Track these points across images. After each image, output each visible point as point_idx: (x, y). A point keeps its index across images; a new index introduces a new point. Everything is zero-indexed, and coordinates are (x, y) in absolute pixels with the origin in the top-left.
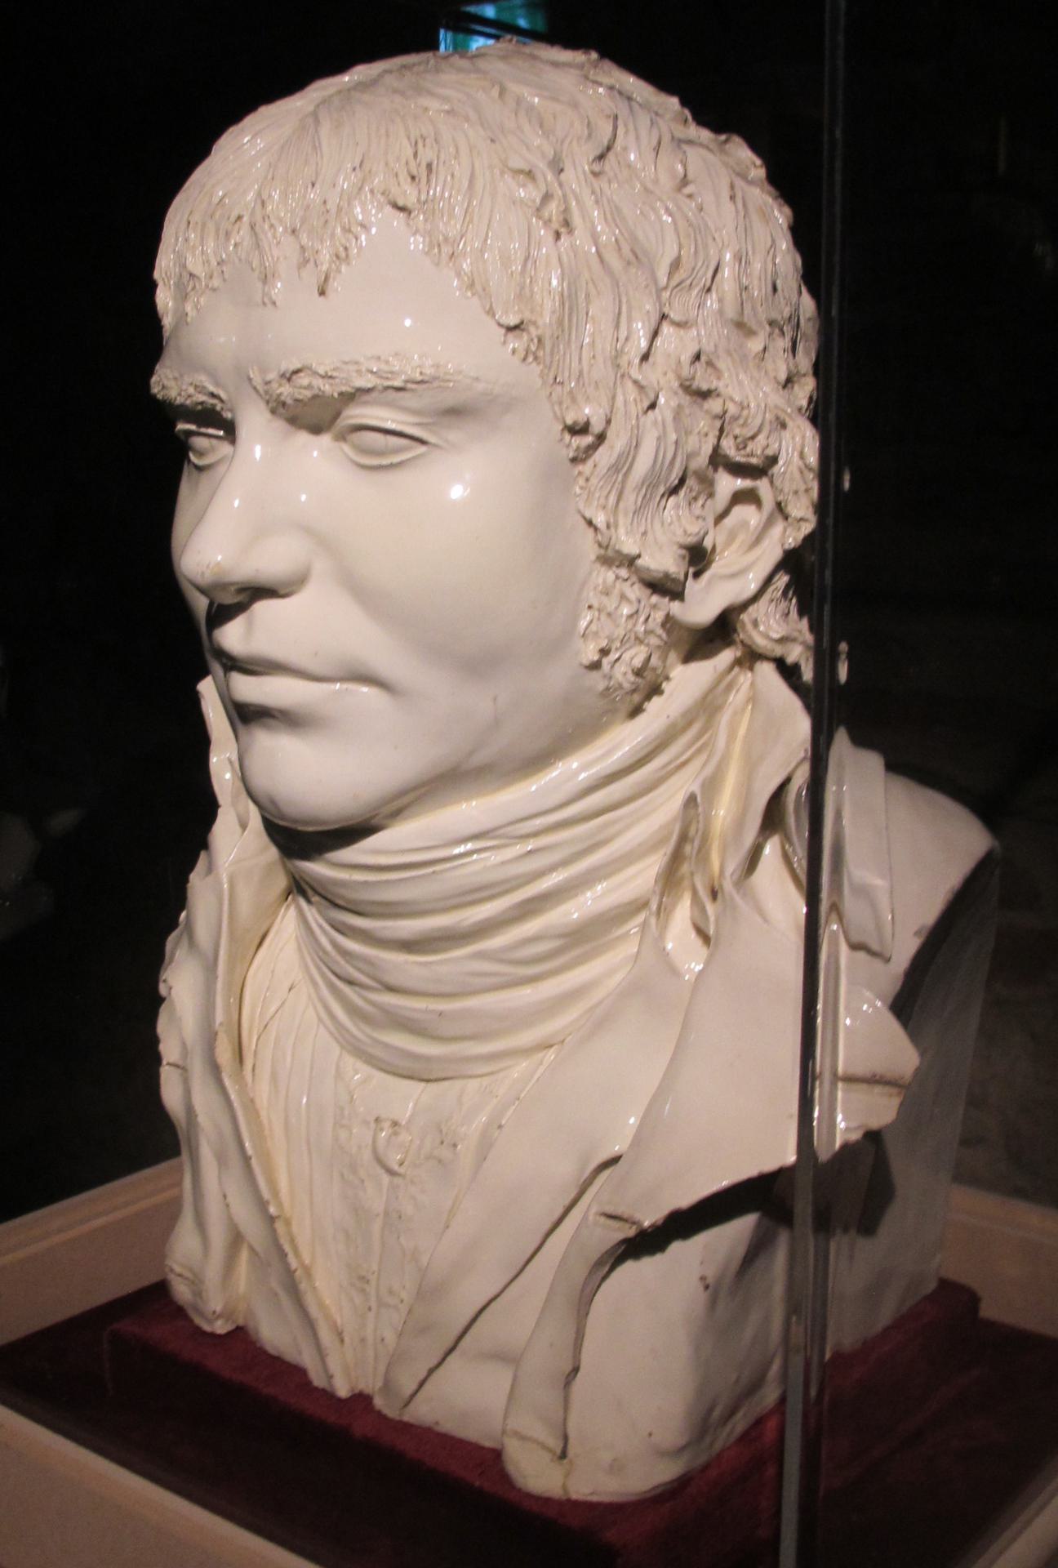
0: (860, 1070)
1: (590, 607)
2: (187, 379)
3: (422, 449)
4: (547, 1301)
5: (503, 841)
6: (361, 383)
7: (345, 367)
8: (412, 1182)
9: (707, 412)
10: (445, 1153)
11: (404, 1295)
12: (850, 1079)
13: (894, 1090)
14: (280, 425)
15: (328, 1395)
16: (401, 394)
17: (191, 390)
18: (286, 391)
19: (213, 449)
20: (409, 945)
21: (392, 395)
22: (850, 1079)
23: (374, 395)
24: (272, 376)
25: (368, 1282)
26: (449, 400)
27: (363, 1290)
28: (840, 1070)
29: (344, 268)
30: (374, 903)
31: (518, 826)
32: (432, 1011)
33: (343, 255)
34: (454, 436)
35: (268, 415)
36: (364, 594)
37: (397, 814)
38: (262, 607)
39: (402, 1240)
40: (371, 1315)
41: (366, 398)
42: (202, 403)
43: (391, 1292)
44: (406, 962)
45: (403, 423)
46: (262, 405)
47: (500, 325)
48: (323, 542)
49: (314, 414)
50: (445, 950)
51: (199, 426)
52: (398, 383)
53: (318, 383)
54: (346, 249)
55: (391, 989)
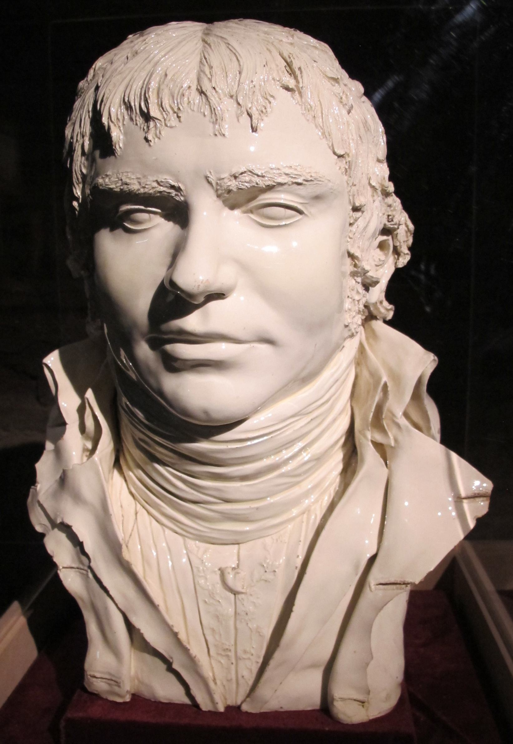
0: (470, 494)
1: (348, 297)
2: (151, 178)
3: (300, 217)
4: (371, 627)
5: (302, 417)
6: (280, 180)
7: (271, 171)
8: (251, 595)
9: (386, 203)
10: (269, 576)
11: (253, 651)
12: (467, 498)
13: (485, 499)
14: (219, 203)
15: (214, 714)
16: (299, 187)
17: (155, 184)
18: (233, 184)
19: (150, 220)
20: (244, 478)
21: (295, 186)
22: (467, 498)
23: (285, 187)
24: (226, 175)
25: (230, 650)
26: (318, 191)
27: (228, 656)
28: (463, 494)
29: (265, 118)
30: (239, 458)
31: (307, 408)
32: (253, 508)
33: (264, 111)
34: (313, 210)
35: (215, 198)
36: (266, 292)
37: (256, 411)
38: (213, 305)
39: (250, 625)
40: (233, 667)
41: (280, 188)
42: (160, 192)
43: (245, 652)
44: (242, 486)
45: (297, 202)
46: (212, 193)
47: (335, 153)
48: (244, 267)
49: (244, 197)
50: (260, 477)
51: (146, 206)
52: (300, 181)
53: (256, 179)
54: (265, 108)
55: (227, 501)
